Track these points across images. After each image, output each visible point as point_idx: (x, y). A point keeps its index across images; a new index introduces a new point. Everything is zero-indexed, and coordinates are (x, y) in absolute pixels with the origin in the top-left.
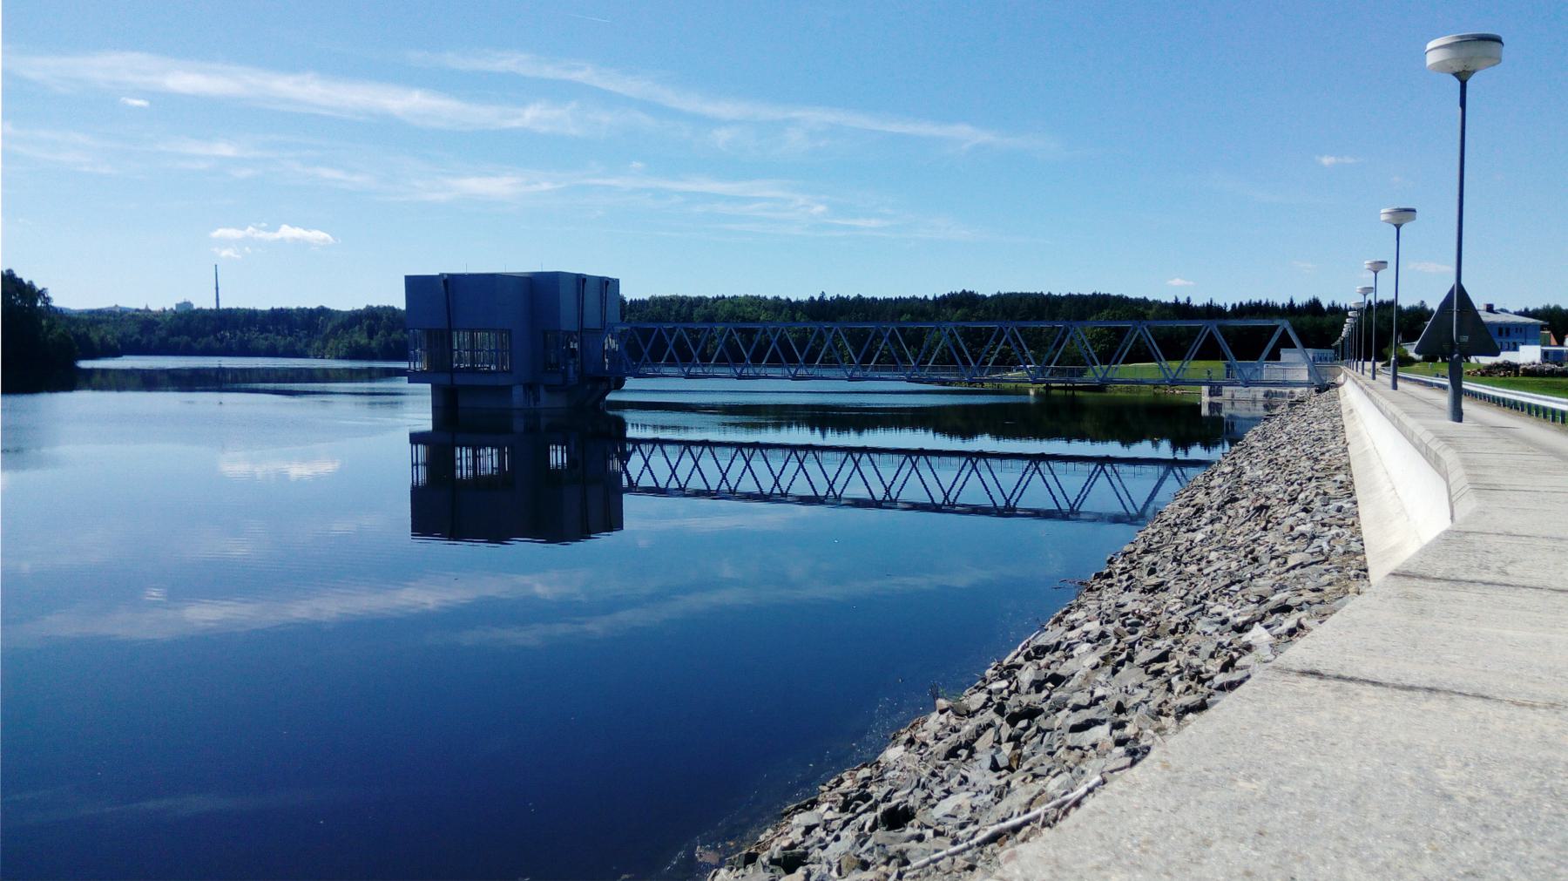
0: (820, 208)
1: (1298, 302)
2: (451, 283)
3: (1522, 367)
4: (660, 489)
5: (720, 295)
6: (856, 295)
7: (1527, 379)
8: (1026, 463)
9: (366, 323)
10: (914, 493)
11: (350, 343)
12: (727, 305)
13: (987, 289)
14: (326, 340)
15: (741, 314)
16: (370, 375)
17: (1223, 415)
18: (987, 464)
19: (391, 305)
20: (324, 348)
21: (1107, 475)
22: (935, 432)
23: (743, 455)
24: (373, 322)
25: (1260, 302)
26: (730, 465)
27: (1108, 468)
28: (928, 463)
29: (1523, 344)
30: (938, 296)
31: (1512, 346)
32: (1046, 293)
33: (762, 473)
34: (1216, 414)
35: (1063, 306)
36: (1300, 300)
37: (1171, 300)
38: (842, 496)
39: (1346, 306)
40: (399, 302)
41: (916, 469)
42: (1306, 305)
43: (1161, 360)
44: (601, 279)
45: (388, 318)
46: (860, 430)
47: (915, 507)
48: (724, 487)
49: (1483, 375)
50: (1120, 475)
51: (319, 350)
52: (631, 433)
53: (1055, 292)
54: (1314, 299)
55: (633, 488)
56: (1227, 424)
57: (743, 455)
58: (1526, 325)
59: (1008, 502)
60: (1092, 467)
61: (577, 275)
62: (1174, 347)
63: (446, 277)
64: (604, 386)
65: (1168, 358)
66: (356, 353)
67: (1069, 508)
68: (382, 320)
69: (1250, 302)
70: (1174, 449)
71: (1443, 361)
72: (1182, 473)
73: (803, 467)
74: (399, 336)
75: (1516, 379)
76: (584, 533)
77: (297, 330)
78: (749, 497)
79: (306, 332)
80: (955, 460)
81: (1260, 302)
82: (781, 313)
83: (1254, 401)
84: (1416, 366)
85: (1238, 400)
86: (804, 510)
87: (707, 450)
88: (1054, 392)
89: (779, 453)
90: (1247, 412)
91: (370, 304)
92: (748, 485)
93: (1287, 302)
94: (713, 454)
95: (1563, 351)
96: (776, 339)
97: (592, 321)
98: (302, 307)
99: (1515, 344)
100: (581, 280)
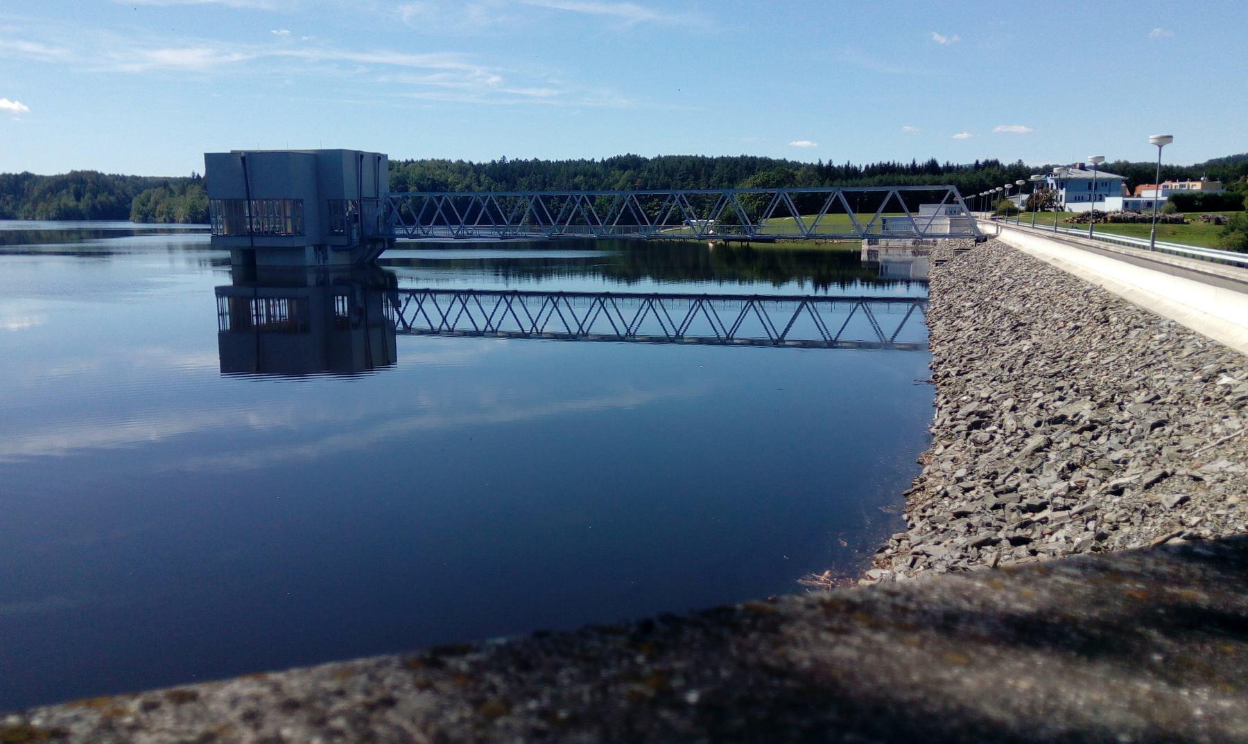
0: (495, 79)
1: (919, 163)
2: (248, 159)
3: (1110, 215)
4: (526, 334)
5: (409, 159)
6: (533, 159)
7: (1115, 225)
8: (693, 302)
9: (72, 187)
10: (555, 326)
11: (59, 205)
12: (417, 169)
13: (649, 152)
14: (35, 203)
15: (431, 177)
16: (80, 235)
17: (879, 260)
18: (613, 302)
19: (94, 170)
20: (35, 211)
21: (755, 309)
22: (604, 277)
23: (416, 299)
24: (79, 186)
25: (889, 163)
26: (449, 309)
27: (756, 303)
28: (661, 304)
29: (1107, 196)
30: (606, 159)
31: (1098, 197)
32: (700, 156)
33: (477, 315)
34: (873, 259)
35: (717, 167)
36: (921, 161)
37: (816, 162)
38: (499, 330)
39: (894, 161)
40: (201, 171)
41: (604, 308)
42: (926, 165)
43: (796, 215)
44: (356, 152)
45: (93, 183)
46: (538, 275)
47: (510, 335)
48: (444, 327)
49: (1078, 222)
50: (765, 309)
51: (29, 212)
52: (402, 285)
53: (709, 155)
54: (932, 160)
55: (408, 330)
56: (882, 266)
57: (416, 299)
58: (1111, 180)
59: (628, 330)
60: (744, 303)
61: (356, 151)
62: (809, 205)
63: (243, 154)
64: (379, 246)
65: (802, 213)
66: (64, 215)
67: (725, 336)
68: (87, 183)
69: (881, 164)
70: (816, 288)
71: (1042, 211)
72: (813, 307)
73: (466, 308)
74: (105, 199)
75: (1104, 225)
76: (369, 367)
77: (4, 194)
78: (466, 334)
79: (12, 196)
80: (587, 300)
81: (889, 163)
82: (465, 175)
83: (905, 248)
84: (1021, 215)
85: (892, 250)
86: (504, 342)
87: (428, 296)
88: (733, 244)
89: (489, 298)
90: (898, 257)
91: (75, 170)
92: (464, 324)
93: (910, 163)
94: (522, 302)
95: (1140, 201)
96: (486, 204)
97: (368, 191)
98: (7, 172)
99: (1101, 195)
100: (359, 156)
